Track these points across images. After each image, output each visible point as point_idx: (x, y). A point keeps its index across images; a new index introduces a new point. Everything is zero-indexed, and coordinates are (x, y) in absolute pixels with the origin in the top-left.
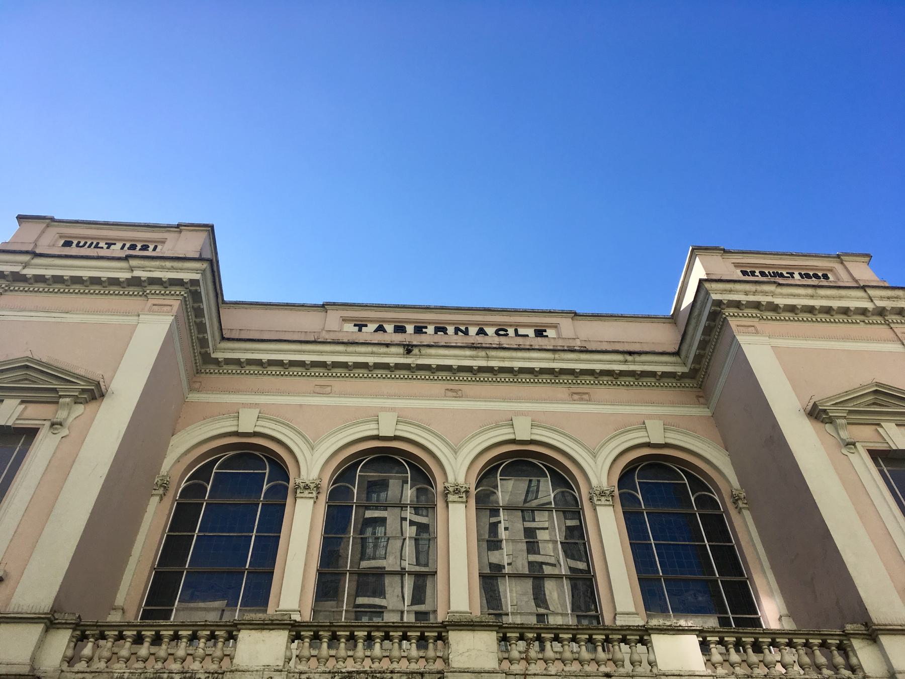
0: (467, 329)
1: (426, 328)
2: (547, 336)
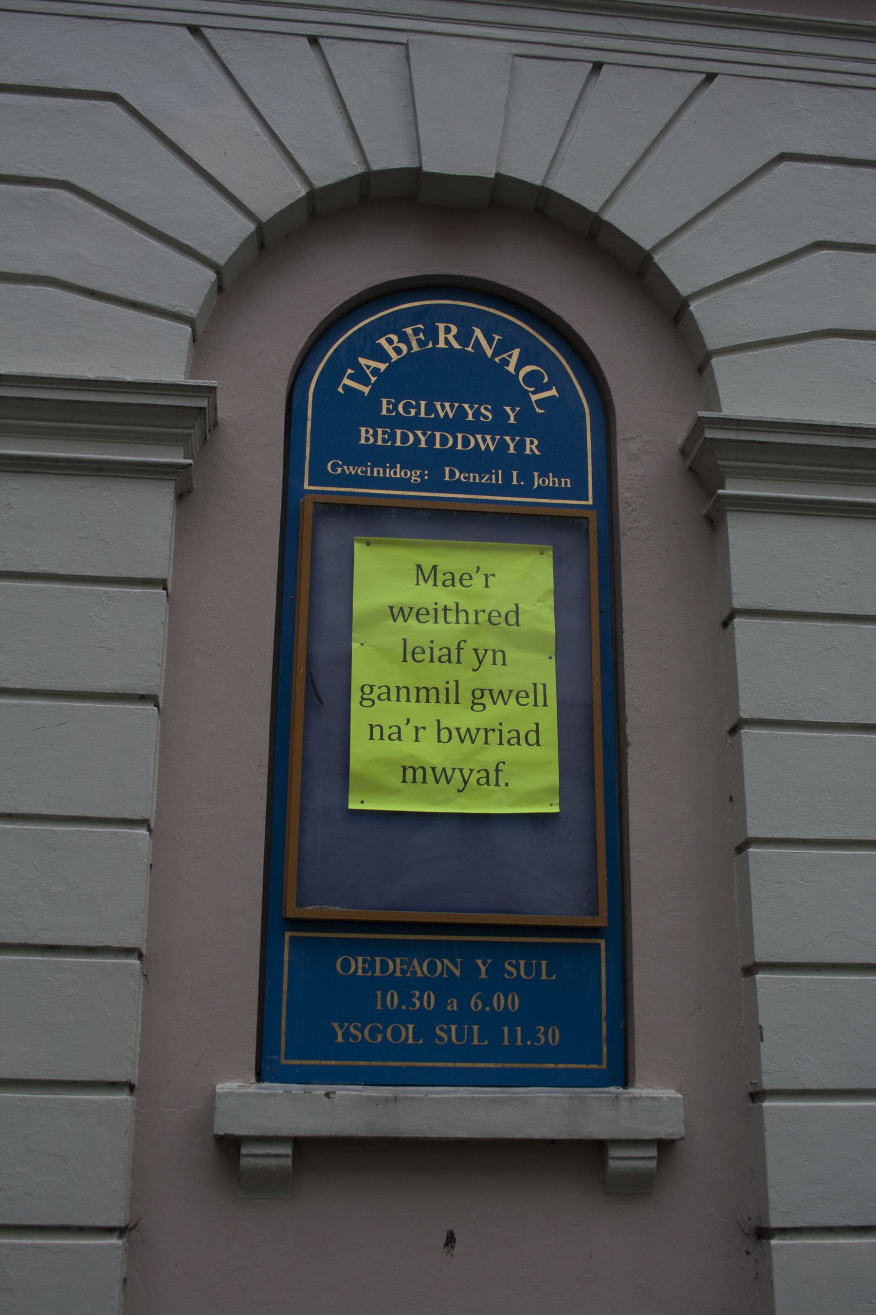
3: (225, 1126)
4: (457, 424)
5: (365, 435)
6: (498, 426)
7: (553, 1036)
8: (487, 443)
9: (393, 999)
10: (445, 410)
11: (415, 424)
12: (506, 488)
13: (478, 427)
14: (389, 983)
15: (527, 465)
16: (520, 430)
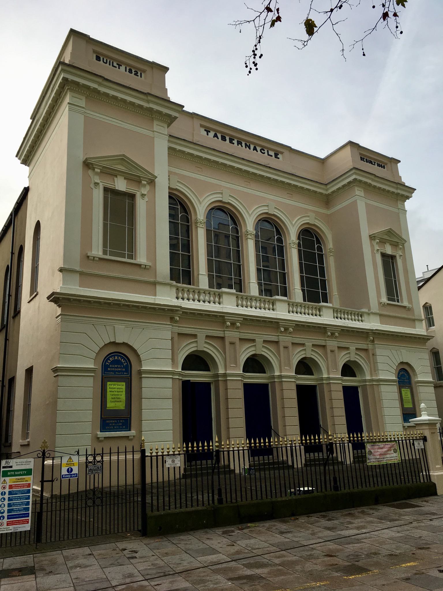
0: (249, 145)
1: (234, 140)
2: (279, 158)
3: (99, 436)
4: (117, 368)
5: (109, 369)
6: (121, 368)
7: (124, 427)
8: (120, 369)
9: (111, 424)
10: (116, 366)
11: (113, 368)
12: (122, 374)
13: (119, 368)
14: (111, 423)
15: (123, 372)
16: (123, 368)
